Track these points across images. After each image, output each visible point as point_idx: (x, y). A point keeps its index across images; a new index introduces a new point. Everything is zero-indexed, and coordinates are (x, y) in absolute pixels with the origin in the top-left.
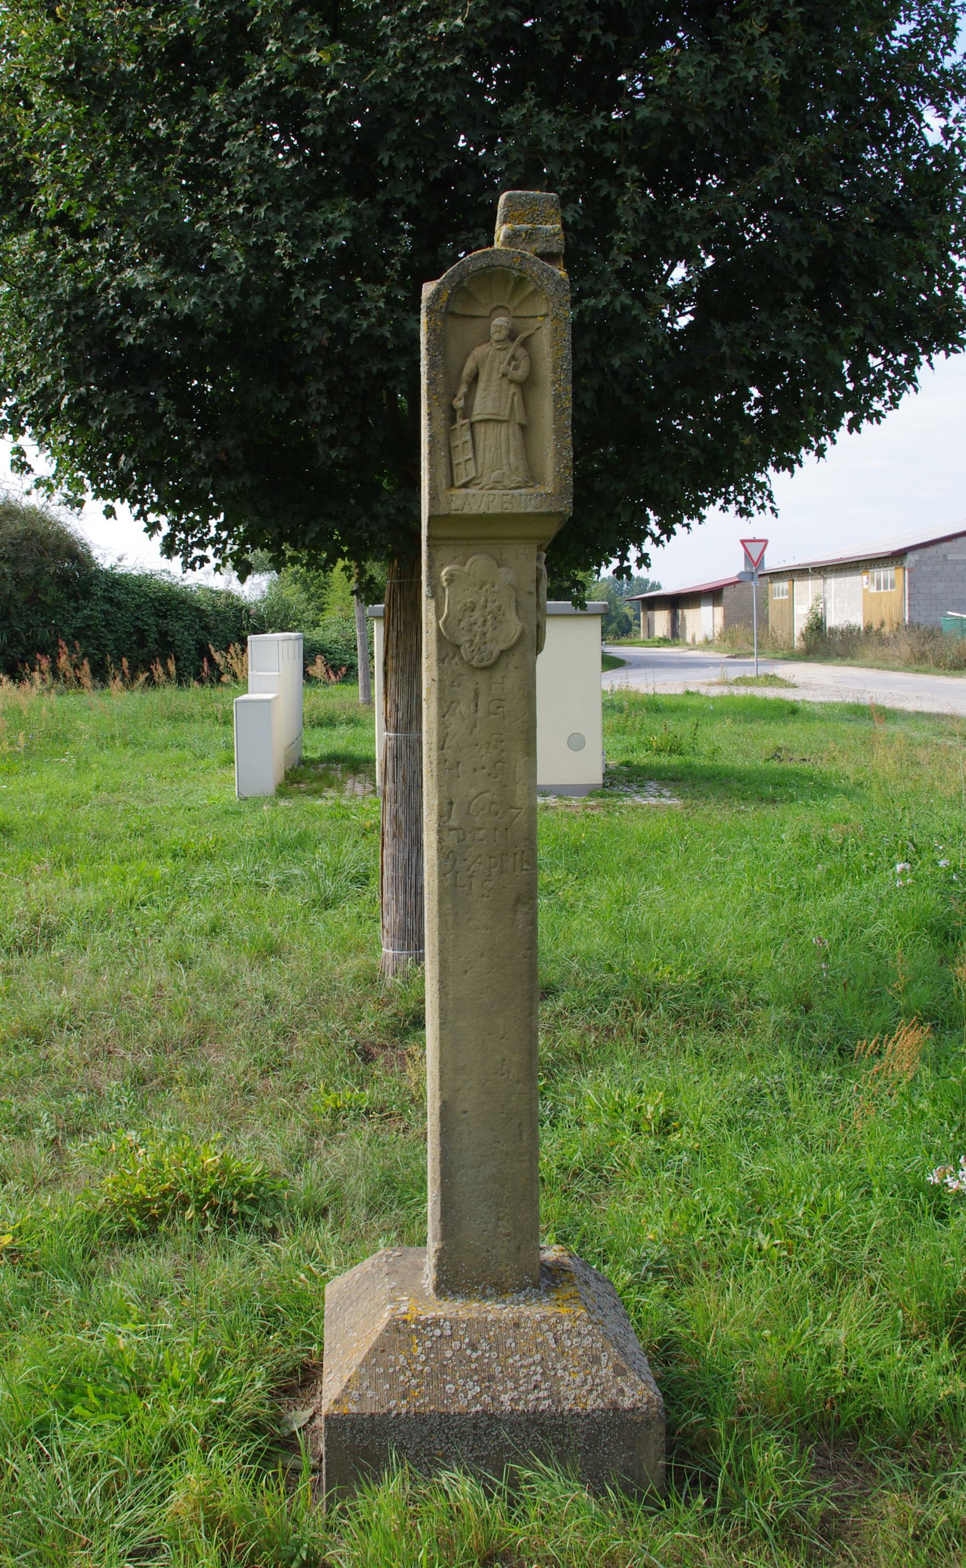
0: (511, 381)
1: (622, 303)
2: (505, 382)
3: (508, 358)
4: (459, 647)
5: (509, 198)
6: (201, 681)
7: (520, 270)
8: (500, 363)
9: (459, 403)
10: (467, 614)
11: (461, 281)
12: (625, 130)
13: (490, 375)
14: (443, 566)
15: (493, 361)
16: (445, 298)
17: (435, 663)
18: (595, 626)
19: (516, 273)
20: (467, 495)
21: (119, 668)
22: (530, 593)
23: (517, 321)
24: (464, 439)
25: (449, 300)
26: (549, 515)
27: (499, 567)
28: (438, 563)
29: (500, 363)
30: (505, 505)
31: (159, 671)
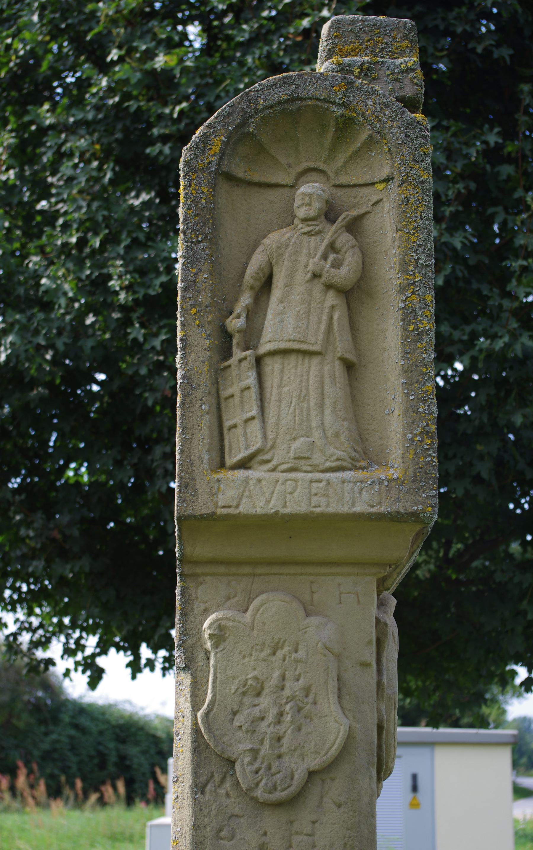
0: (329, 287)
1: (523, 344)
2: (318, 287)
3: (323, 247)
4: (232, 763)
5: (336, 25)
6: (148, 802)
7: (345, 105)
8: (310, 256)
9: (236, 323)
10: (247, 700)
11: (244, 123)
12: (523, 149)
13: (292, 272)
14: (206, 612)
15: (297, 252)
16: (216, 149)
17: (187, 791)
18: (504, 757)
19: (338, 111)
20: (247, 480)
21: (73, 786)
22: (365, 665)
23: (340, 193)
24: (243, 384)
25: (222, 153)
26: (396, 518)
27: (308, 614)
28: (198, 607)
29: (310, 256)
30: (315, 500)
31: (108, 791)
